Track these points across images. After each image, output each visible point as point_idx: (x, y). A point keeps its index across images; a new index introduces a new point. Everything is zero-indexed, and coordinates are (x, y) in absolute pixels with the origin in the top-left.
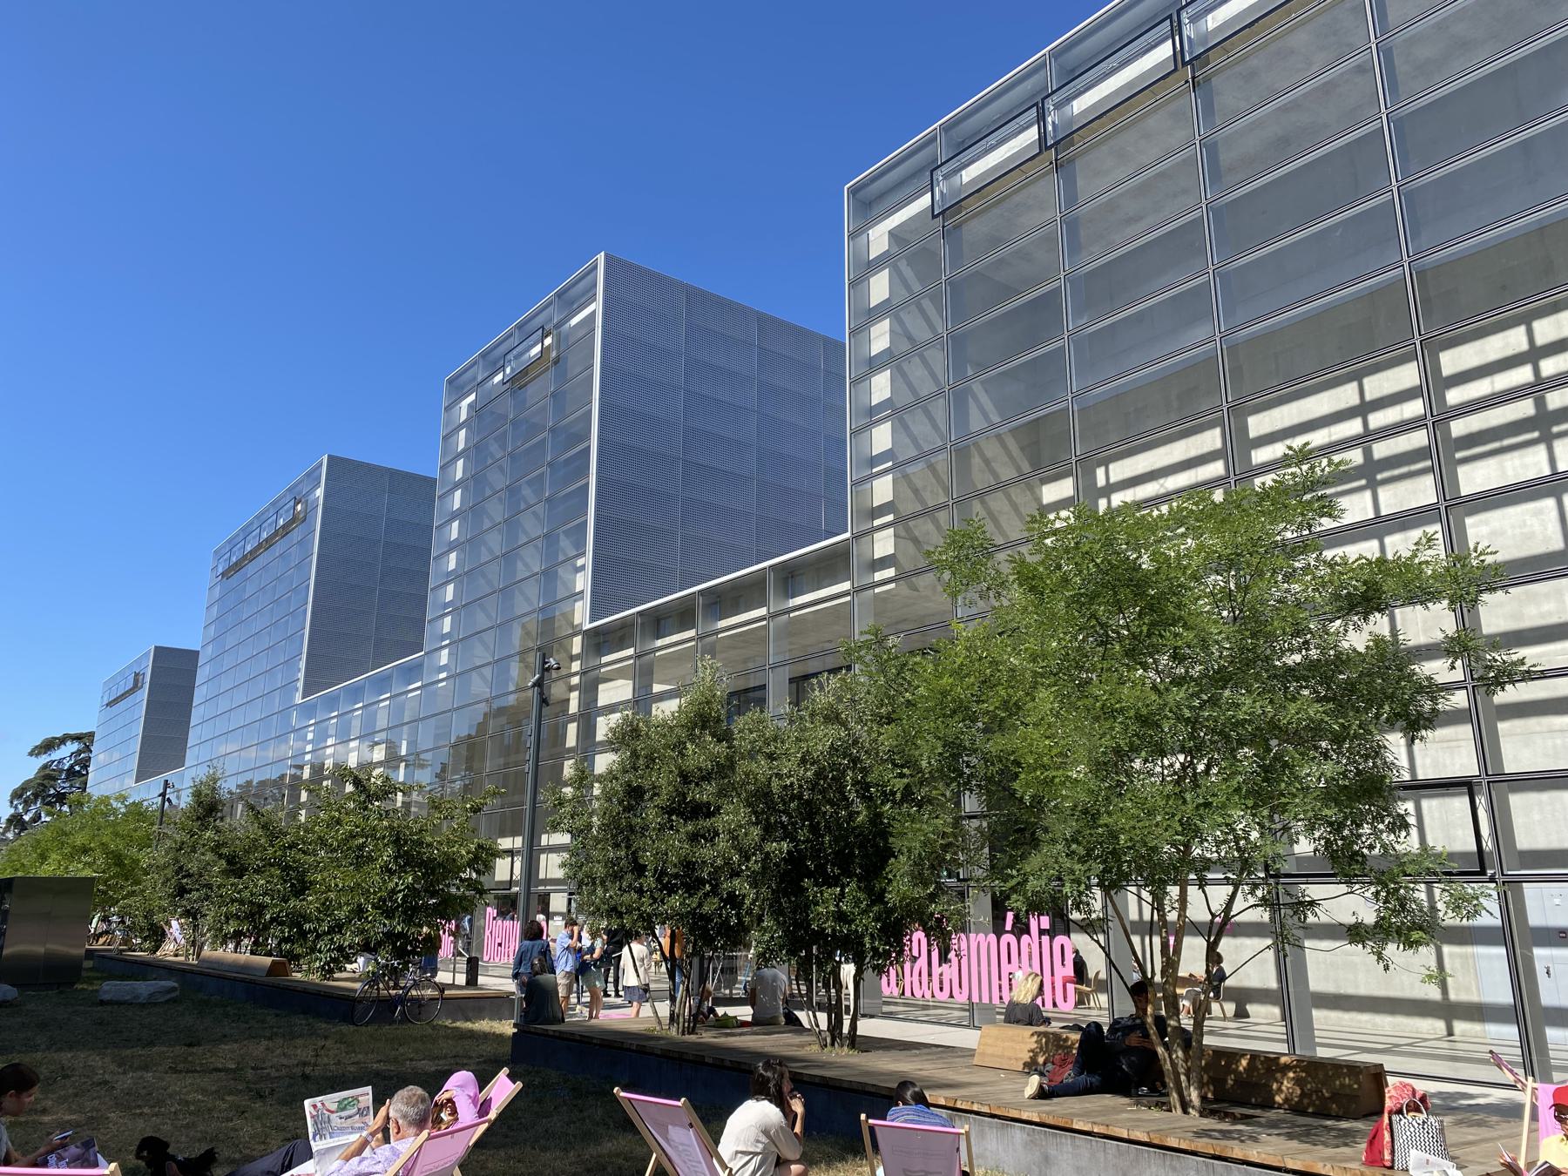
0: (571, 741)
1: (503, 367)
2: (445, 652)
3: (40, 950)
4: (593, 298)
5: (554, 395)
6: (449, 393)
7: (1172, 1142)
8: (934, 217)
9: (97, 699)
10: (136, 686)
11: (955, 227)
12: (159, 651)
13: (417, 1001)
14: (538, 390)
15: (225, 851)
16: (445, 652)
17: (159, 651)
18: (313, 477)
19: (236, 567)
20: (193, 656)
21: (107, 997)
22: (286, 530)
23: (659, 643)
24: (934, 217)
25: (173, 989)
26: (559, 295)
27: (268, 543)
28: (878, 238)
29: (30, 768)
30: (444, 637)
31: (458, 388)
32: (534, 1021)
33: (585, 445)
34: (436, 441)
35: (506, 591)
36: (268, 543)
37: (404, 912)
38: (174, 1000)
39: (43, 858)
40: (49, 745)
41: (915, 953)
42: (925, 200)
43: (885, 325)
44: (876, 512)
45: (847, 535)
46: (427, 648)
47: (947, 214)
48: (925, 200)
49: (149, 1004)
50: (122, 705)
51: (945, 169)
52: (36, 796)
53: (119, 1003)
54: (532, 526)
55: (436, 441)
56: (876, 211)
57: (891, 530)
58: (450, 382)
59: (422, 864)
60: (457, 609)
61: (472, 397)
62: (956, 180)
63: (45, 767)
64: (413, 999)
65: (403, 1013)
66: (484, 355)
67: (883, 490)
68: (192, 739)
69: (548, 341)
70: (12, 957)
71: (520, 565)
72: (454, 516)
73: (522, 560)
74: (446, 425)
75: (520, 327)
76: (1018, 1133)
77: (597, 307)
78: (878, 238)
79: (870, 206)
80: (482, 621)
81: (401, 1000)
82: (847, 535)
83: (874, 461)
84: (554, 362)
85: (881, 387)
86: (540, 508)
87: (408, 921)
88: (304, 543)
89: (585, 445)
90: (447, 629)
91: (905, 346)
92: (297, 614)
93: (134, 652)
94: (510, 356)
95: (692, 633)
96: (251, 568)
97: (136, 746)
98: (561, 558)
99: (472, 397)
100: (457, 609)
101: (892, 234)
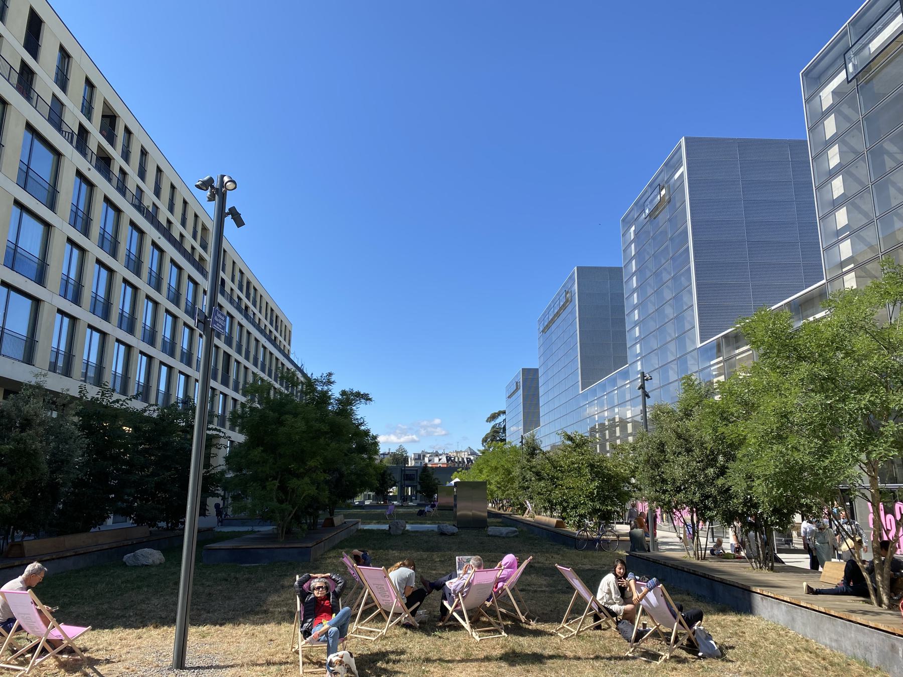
0: (618, 429)
1: (644, 210)
2: (639, 363)
3: (470, 513)
4: (681, 165)
5: (670, 220)
6: (623, 227)
7: (833, 613)
8: (849, 82)
9: (504, 395)
10: (517, 389)
11: (867, 83)
12: (523, 369)
13: (605, 541)
14: (664, 216)
15: (533, 470)
16: (639, 363)
17: (523, 369)
18: (571, 278)
19: (547, 327)
20: (537, 370)
21: (490, 533)
22: (564, 307)
23: (737, 351)
24: (849, 82)
25: (515, 531)
26: (666, 165)
27: (558, 315)
28: (826, 96)
29: (488, 428)
30: (637, 355)
31: (627, 223)
32: (634, 551)
33: (685, 247)
34: (622, 250)
35: (661, 329)
36: (558, 315)
37: (600, 499)
38: (517, 536)
39: (481, 471)
40: (494, 417)
41: (889, 528)
42: (842, 76)
43: (836, 148)
44: (842, 264)
45: (824, 281)
46: (629, 362)
47: (863, 77)
48: (842, 76)
49: (507, 537)
50: (514, 397)
51: (854, 49)
52: (492, 441)
53: (495, 536)
54: (668, 294)
55: (622, 250)
56: (823, 81)
57: (853, 274)
58: (623, 221)
59: (604, 476)
60: (642, 340)
61: (633, 228)
62: (865, 52)
63: (494, 427)
64: (604, 540)
65: (600, 546)
66: (636, 204)
67: (846, 249)
68: (542, 411)
69: (663, 192)
70: (461, 516)
71: (892, 191)
72: (634, 291)
73: (894, 184)
74: (624, 243)
75: (650, 185)
76: (783, 606)
77: (683, 169)
78: (826, 96)
79: (817, 79)
80: (654, 345)
81: (599, 540)
82: (824, 281)
83: (838, 233)
84: (669, 201)
85: (838, 187)
86: (669, 283)
87: (602, 503)
88: (572, 312)
89: (685, 247)
90: (638, 351)
91: (852, 156)
92: (574, 348)
93: (514, 374)
94: (647, 202)
95: (721, 358)
96: (554, 327)
97: (521, 417)
98: (685, 308)
99: (633, 228)
100: (642, 340)
101: (834, 93)
